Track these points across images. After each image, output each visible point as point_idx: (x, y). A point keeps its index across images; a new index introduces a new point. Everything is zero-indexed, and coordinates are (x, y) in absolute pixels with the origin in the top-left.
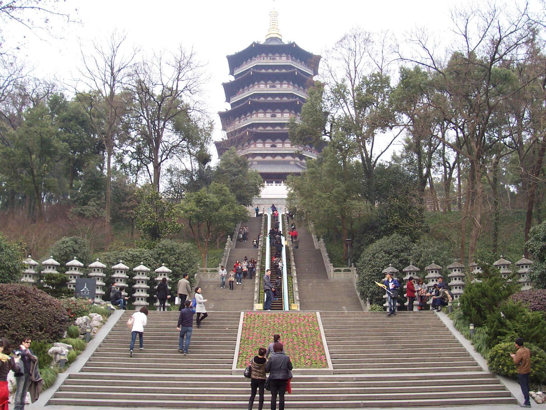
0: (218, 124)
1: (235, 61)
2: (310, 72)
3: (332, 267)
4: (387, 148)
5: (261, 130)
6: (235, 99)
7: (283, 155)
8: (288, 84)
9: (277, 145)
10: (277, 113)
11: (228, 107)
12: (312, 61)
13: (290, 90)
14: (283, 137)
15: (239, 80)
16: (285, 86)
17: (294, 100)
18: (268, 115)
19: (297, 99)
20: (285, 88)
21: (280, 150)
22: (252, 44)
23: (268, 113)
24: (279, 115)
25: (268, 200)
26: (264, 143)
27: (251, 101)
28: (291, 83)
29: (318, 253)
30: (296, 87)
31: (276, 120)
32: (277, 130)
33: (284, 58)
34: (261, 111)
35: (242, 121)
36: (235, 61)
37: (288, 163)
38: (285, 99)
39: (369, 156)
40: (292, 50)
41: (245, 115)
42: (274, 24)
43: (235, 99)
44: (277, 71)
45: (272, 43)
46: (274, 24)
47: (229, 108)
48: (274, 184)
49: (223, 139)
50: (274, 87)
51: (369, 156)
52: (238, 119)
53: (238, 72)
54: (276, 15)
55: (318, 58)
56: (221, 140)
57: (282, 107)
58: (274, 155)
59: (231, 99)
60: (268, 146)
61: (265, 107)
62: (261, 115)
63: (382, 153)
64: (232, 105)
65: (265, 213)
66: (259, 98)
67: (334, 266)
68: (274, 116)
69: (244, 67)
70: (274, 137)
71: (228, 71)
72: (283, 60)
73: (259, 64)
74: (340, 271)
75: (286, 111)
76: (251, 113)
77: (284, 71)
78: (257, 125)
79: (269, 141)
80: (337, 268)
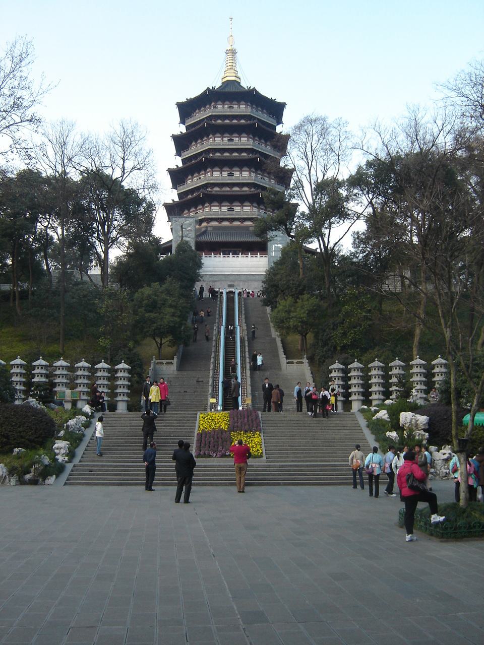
0: (167, 181)
1: (186, 109)
2: (271, 121)
4: (348, 231)
5: (216, 191)
6: (187, 154)
9: (235, 208)
10: (234, 105)
11: (183, 129)
12: (276, 109)
15: (187, 167)
16: (244, 140)
17: (252, 122)
18: (226, 139)
23: (225, 171)
24: (236, 140)
25: (223, 277)
26: (220, 206)
27: (205, 158)
30: (254, 108)
31: (233, 180)
32: (234, 191)
33: (243, 107)
35: (195, 179)
36: (186, 109)
38: (244, 154)
39: (326, 245)
40: (253, 97)
43: (187, 154)
44: (235, 121)
46: (232, 68)
47: (184, 131)
48: (231, 255)
49: (173, 200)
51: (326, 245)
54: (232, 52)
55: (282, 106)
56: (172, 202)
57: (240, 164)
62: (218, 140)
63: (340, 240)
65: (220, 291)
67: (287, 358)
68: (231, 107)
70: (232, 199)
71: (178, 119)
72: (242, 109)
73: (214, 114)
74: (292, 363)
75: (244, 135)
76: (208, 136)
77: (243, 121)
80: (289, 360)
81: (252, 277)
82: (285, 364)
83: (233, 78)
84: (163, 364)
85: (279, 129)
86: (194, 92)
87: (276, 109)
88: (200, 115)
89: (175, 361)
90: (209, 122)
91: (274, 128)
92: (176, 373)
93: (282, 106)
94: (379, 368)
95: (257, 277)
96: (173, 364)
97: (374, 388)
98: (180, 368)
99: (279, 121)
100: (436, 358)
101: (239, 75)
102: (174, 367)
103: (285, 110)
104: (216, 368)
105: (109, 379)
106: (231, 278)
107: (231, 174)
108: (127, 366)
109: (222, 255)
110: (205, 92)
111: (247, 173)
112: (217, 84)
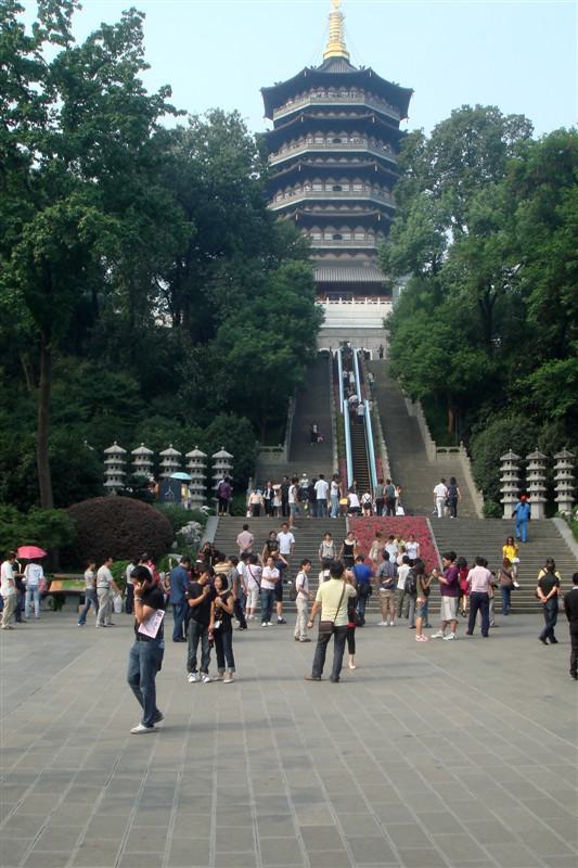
2: (393, 115)
3: (434, 446)
5: (317, 212)
7: (353, 252)
8: (361, 137)
12: (399, 98)
13: (364, 148)
14: (353, 223)
17: (370, 163)
18: (329, 188)
19: (375, 162)
20: (357, 191)
21: (348, 244)
22: (303, 72)
28: (365, 135)
29: (413, 421)
34: (319, 133)
37: (359, 265)
40: (367, 81)
41: (292, 186)
42: (338, 38)
44: (343, 115)
45: (334, 70)
46: (338, 38)
47: (272, 128)
50: (337, 141)
52: (280, 192)
53: (280, 114)
54: (341, 17)
55: (408, 93)
58: (338, 252)
59: (275, 114)
60: (329, 236)
61: (323, 174)
64: (276, 124)
66: (316, 114)
67: (437, 445)
69: (253, 599)
70: (338, 223)
71: (262, 110)
72: (351, 99)
75: (358, 180)
76: (302, 183)
77: (353, 115)
78: (312, 203)
79: (330, 228)
81: (333, 332)
82: (434, 453)
83: (340, 54)
84: (445, 451)
85: (403, 126)
86: (287, 74)
87: (399, 98)
88: (293, 107)
89: (285, 448)
90: (307, 115)
91: (397, 124)
92: (286, 462)
93: (408, 93)
94: (514, 462)
95: (359, 332)
96: (282, 451)
97: (561, 487)
98: (292, 457)
99: (404, 115)
100: (193, 448)
101: (348, 49)
102: (284, 457)
103: (412, 100)
104: (342, 457)
105: (123, 468)
106: (345, 333)
107: (337, 189)
108: (228, 455)
109: (340, 301)
110: (301, 74)
111: (360, 187)
112: (317, 63)
